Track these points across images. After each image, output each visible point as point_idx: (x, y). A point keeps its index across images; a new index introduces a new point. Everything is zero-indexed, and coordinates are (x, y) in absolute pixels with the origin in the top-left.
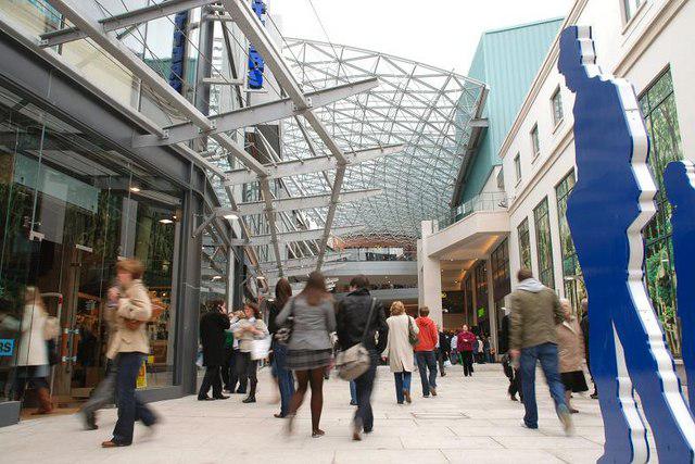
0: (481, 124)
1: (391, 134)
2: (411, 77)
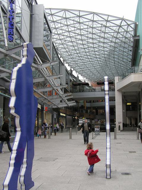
0: (137, 38)
1: (105, 33)
2: (107, 21)
